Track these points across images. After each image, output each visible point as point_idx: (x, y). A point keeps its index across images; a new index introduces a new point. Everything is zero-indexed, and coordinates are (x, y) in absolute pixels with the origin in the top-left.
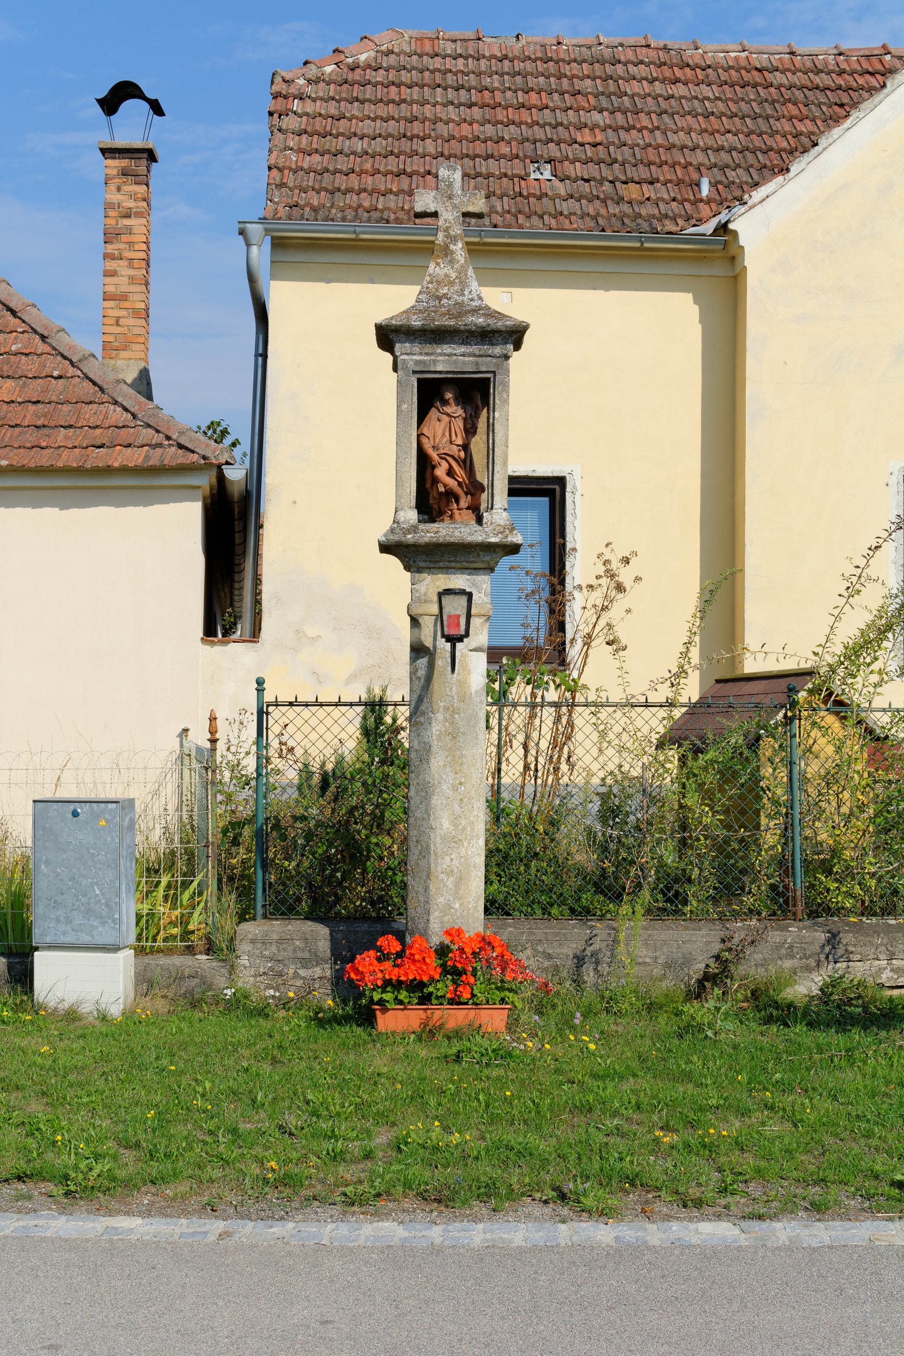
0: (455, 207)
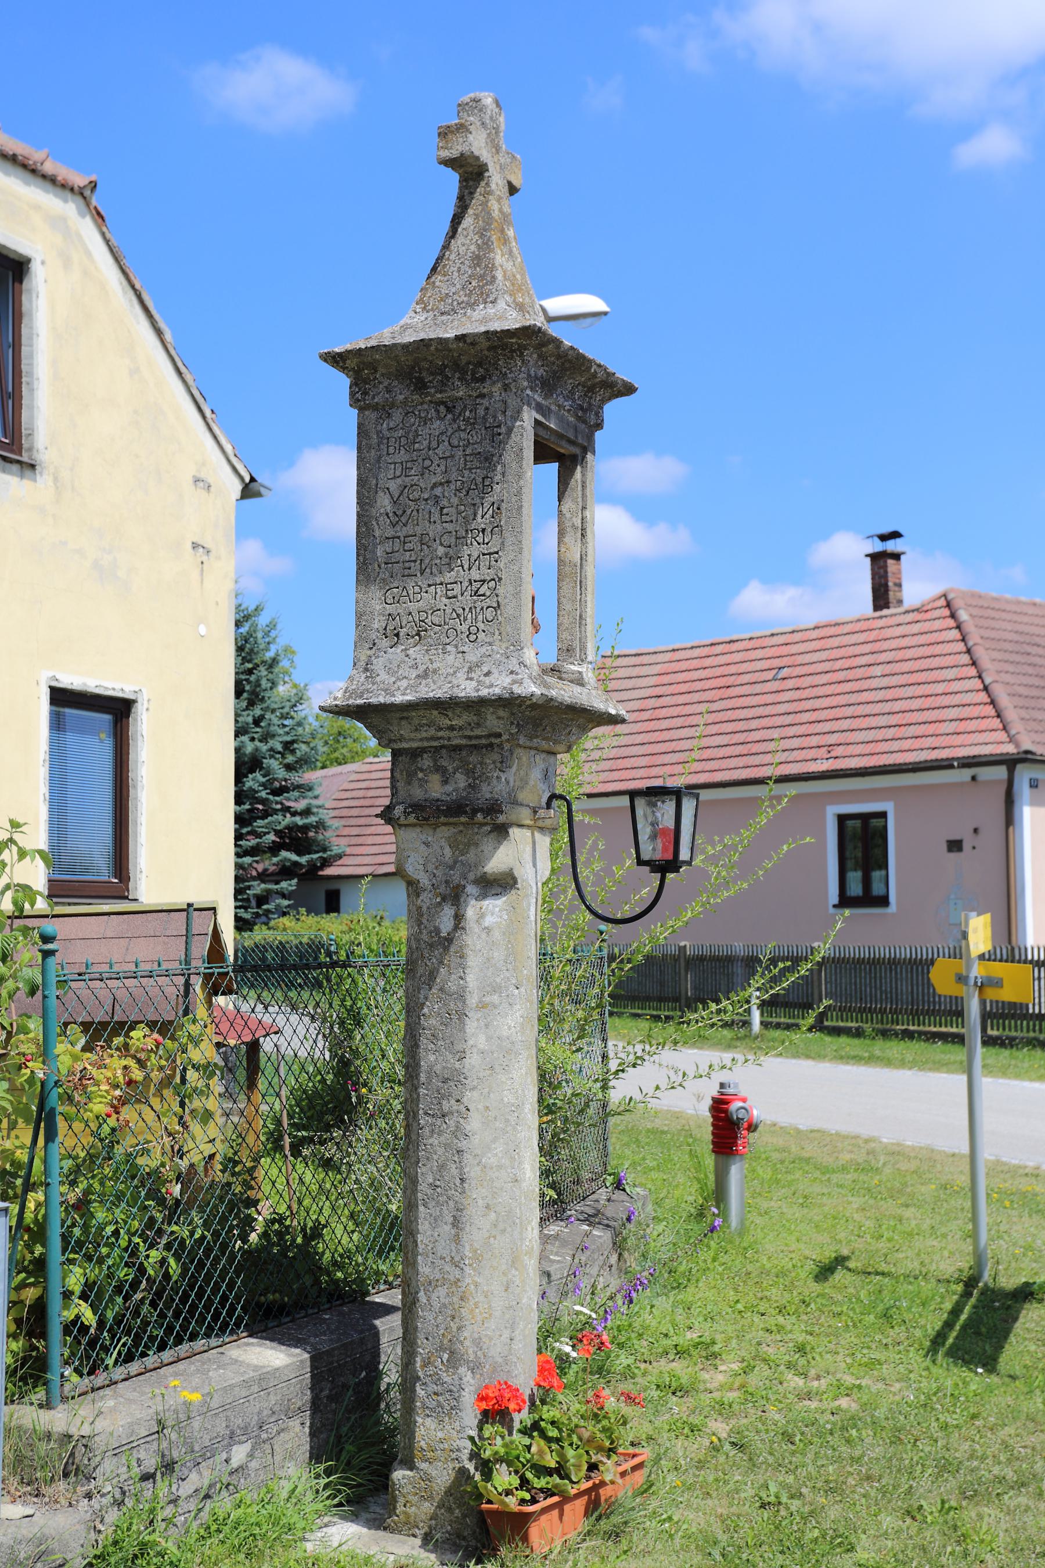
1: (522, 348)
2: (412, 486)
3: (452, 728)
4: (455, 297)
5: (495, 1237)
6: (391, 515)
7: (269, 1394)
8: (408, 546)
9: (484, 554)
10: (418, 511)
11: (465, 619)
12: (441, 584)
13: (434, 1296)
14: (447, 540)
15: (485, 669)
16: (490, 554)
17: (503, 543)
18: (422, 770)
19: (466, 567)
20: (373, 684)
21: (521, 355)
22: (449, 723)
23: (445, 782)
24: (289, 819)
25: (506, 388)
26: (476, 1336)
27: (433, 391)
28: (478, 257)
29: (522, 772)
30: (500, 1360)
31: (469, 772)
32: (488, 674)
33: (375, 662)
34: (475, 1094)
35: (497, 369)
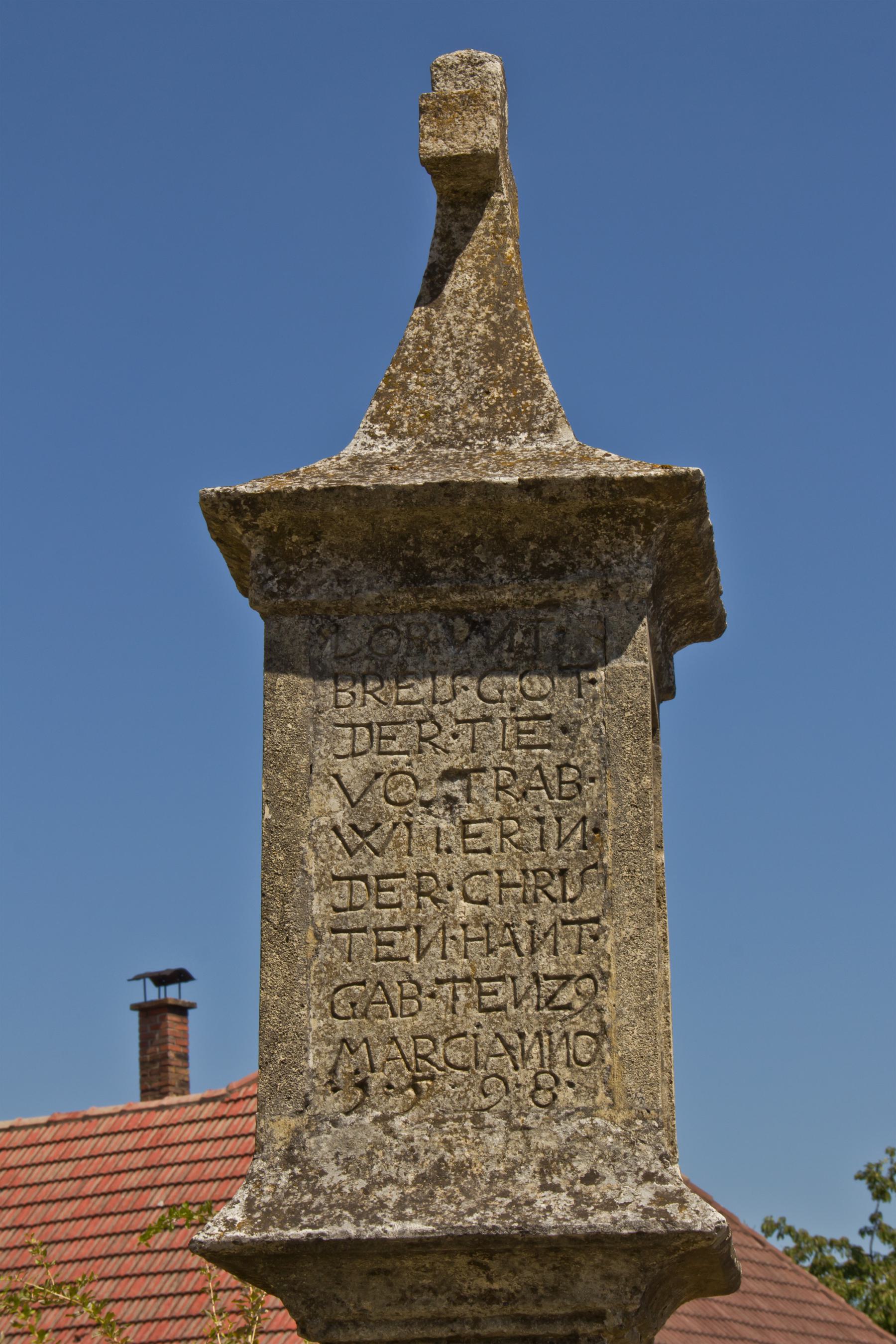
2: (393, 774)
3: (489, 1297)
4: (458, 415)
6: (344, 830)
8: (386, 896)
9: (565, 922)
10: (408, 825)
11: (526, 1056)
12: (467, 979)
14: (476, 888)
15: (583, 1168)
16: (580, 922)
17: (609, 902)
19: (524, 946)
20: (316, 1192)
22: (485, 1284)
25: (608, 592)
27: (444, 587)
28: (495, 345)
32: (591, 1178)
33: (311, 1143)
35: (589, 554)
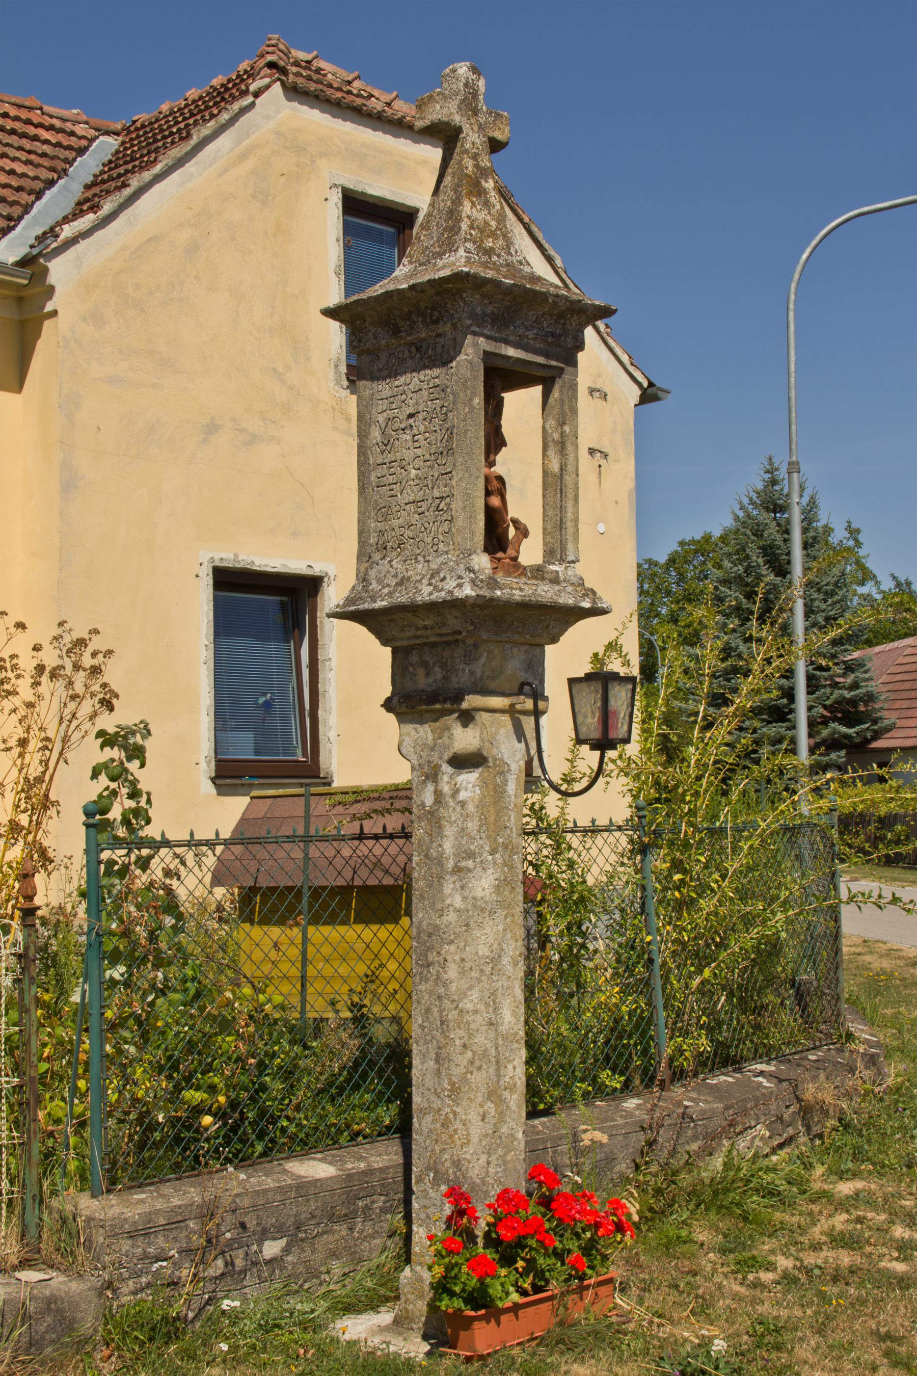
0: (480, 127)
1: (460, 292)
3: (426, 628)
5: (472, 1073)
7: (308, 1200)
13: (423, 1123)
15: (442, 575)
17: (454, 464)
18: (412, 665)
21: (461, 297)
23: (427, 675)
24: (837, 693)
25: (454, 327)
26: (455, 1158)
29: (493, 664)
30: (478, 1181)
31: (444, 666)
34: (452, 948)
